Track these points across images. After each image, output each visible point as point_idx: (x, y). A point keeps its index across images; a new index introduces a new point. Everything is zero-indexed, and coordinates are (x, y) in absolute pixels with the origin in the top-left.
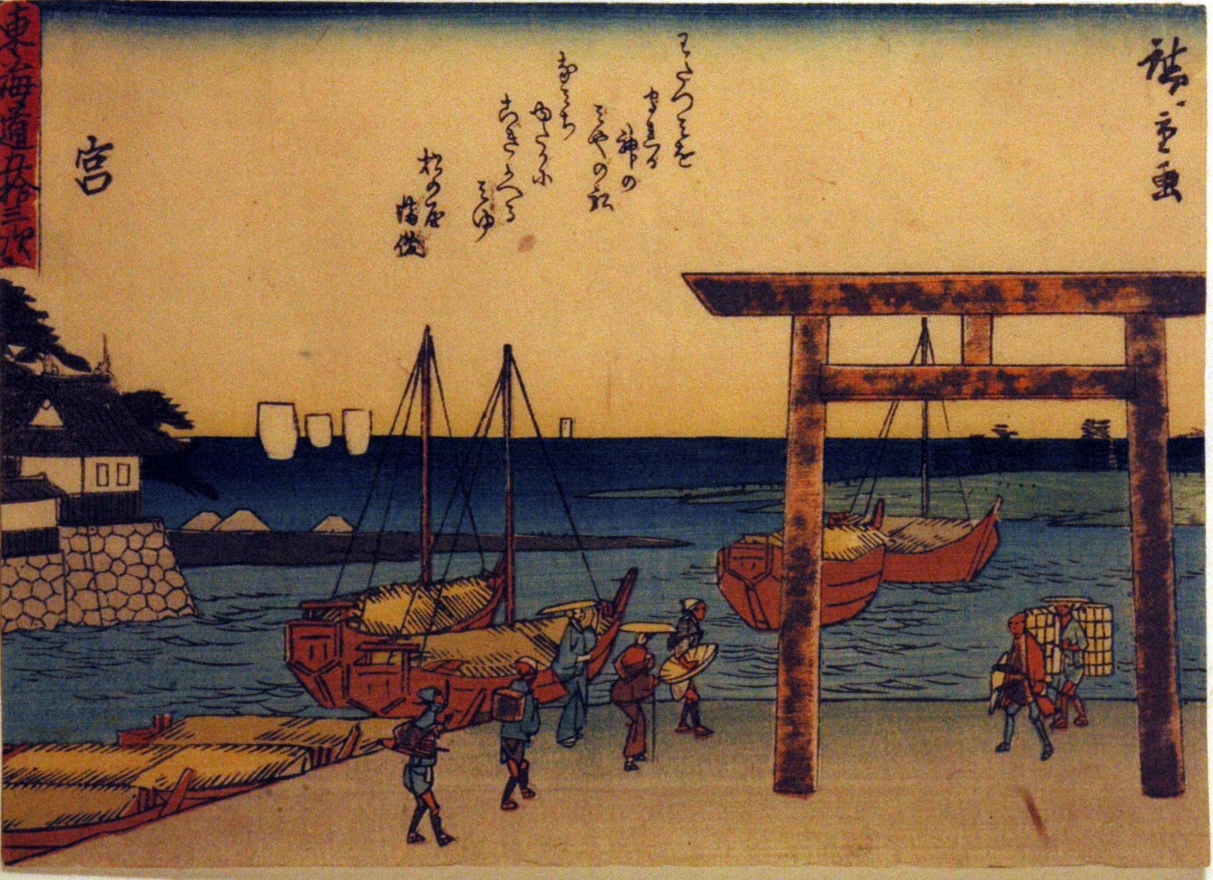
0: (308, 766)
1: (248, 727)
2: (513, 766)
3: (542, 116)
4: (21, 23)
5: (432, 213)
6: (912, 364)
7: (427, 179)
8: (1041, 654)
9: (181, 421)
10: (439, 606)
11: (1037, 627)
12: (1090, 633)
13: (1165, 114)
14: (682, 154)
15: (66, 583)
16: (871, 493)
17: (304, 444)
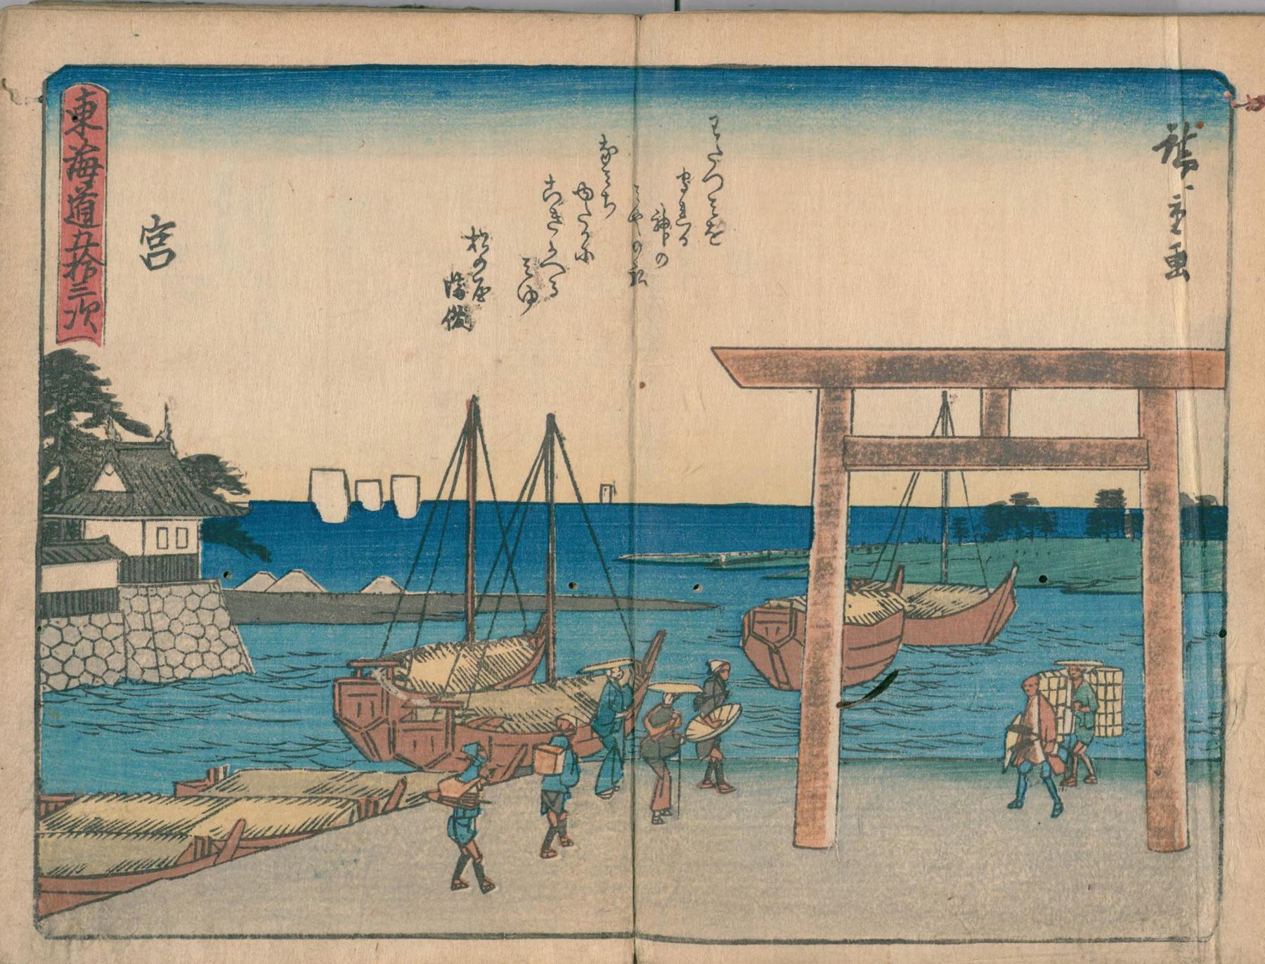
0: (355, 818)
1: (302, 777)
2: (553, 817)
3: (584, 196)
4: (88, 107)
5: (479, 288)
6: (933, 436)
7: (473, 256)
8: (1052, 716)
9: (235, 484)
10: (481, 664)
11: (1050, 689)
12: (1101, 695)
13: (1177, 197)
14: (713, 232)
15: (126, 641)
16: (892, 561)
17: (356, 507)
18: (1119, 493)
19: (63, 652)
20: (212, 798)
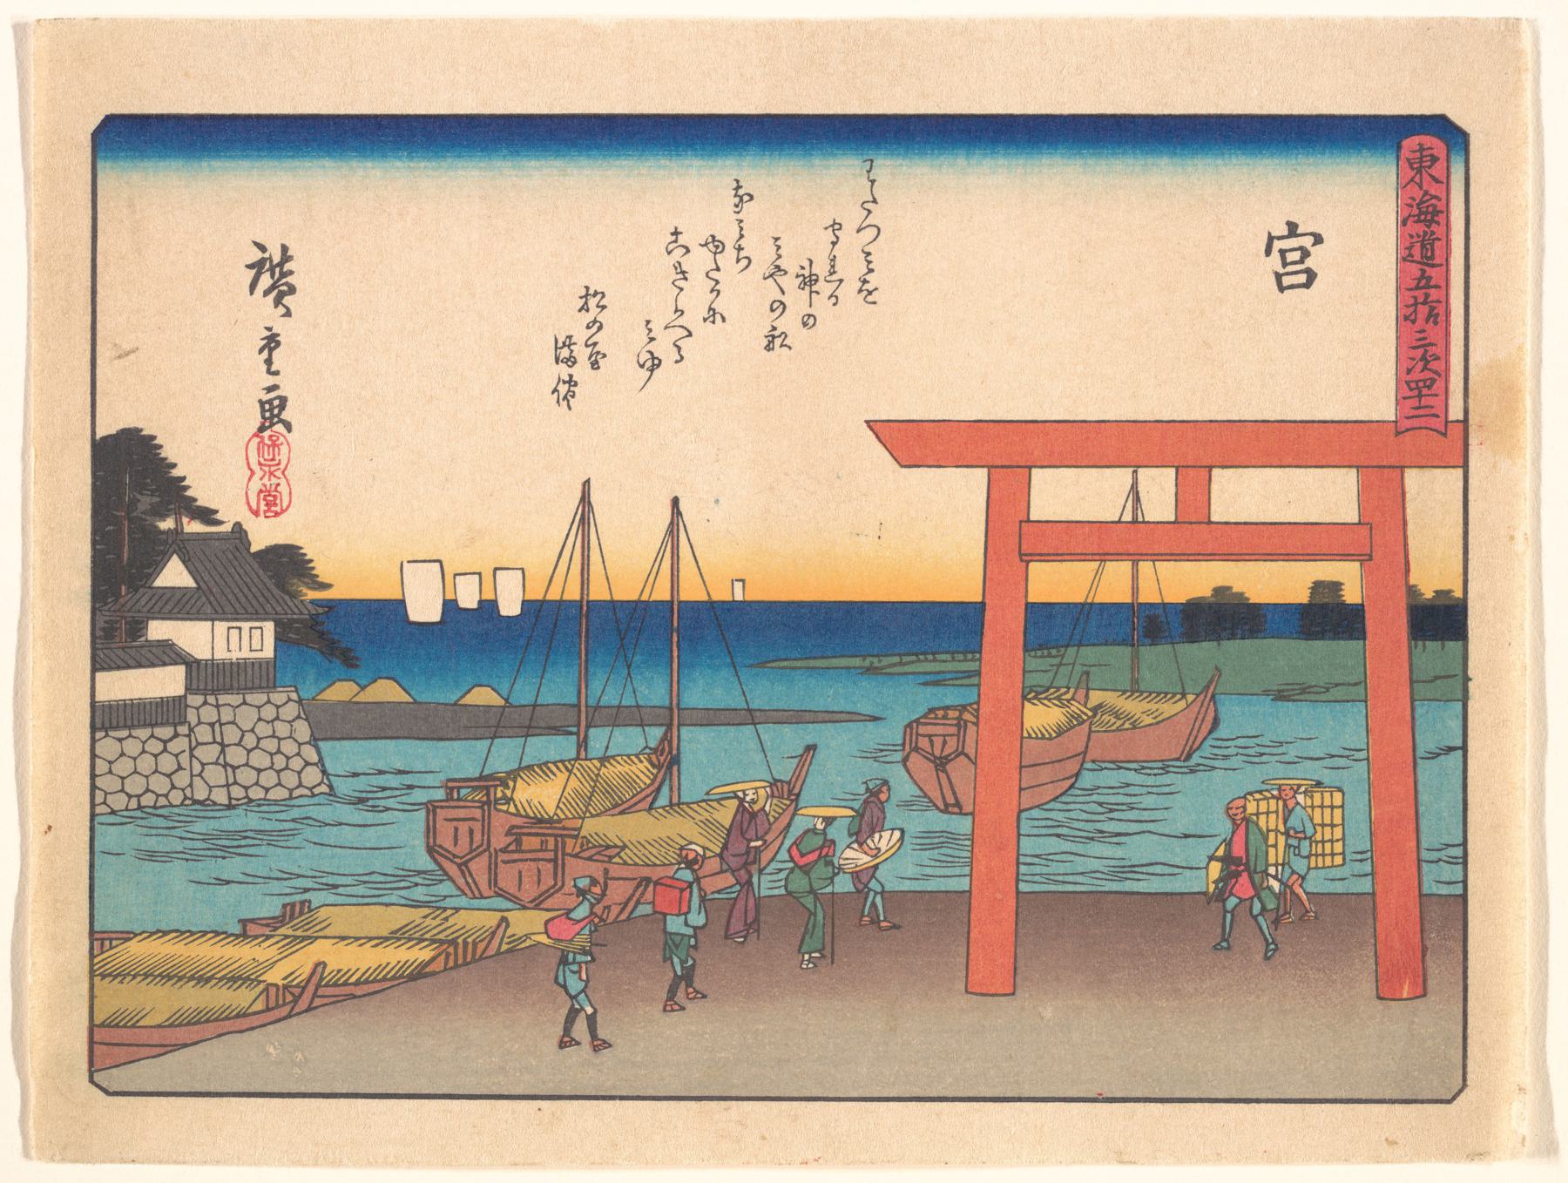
12: (1317, 820)
15: (192, 756)
17: (450, 606)
18: (1336, 586)
19: (124, 767)
20: (286, 937)
